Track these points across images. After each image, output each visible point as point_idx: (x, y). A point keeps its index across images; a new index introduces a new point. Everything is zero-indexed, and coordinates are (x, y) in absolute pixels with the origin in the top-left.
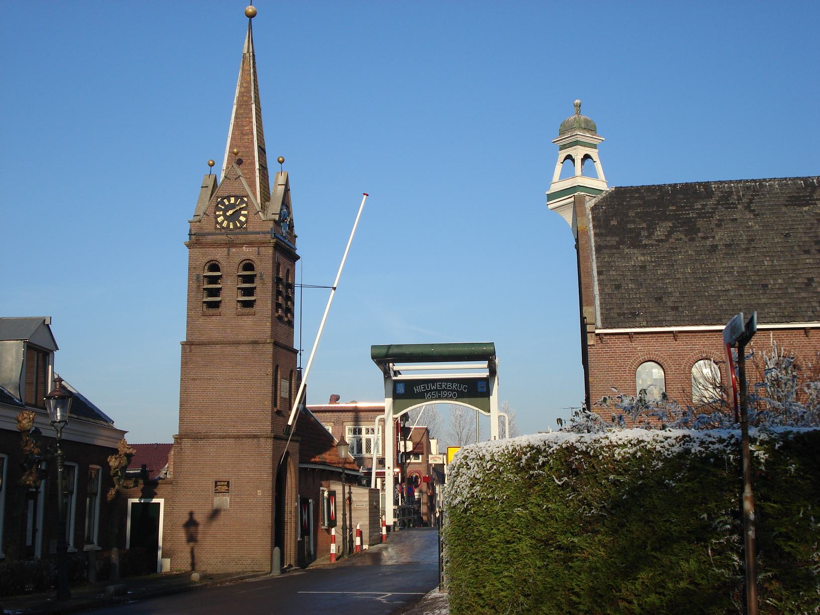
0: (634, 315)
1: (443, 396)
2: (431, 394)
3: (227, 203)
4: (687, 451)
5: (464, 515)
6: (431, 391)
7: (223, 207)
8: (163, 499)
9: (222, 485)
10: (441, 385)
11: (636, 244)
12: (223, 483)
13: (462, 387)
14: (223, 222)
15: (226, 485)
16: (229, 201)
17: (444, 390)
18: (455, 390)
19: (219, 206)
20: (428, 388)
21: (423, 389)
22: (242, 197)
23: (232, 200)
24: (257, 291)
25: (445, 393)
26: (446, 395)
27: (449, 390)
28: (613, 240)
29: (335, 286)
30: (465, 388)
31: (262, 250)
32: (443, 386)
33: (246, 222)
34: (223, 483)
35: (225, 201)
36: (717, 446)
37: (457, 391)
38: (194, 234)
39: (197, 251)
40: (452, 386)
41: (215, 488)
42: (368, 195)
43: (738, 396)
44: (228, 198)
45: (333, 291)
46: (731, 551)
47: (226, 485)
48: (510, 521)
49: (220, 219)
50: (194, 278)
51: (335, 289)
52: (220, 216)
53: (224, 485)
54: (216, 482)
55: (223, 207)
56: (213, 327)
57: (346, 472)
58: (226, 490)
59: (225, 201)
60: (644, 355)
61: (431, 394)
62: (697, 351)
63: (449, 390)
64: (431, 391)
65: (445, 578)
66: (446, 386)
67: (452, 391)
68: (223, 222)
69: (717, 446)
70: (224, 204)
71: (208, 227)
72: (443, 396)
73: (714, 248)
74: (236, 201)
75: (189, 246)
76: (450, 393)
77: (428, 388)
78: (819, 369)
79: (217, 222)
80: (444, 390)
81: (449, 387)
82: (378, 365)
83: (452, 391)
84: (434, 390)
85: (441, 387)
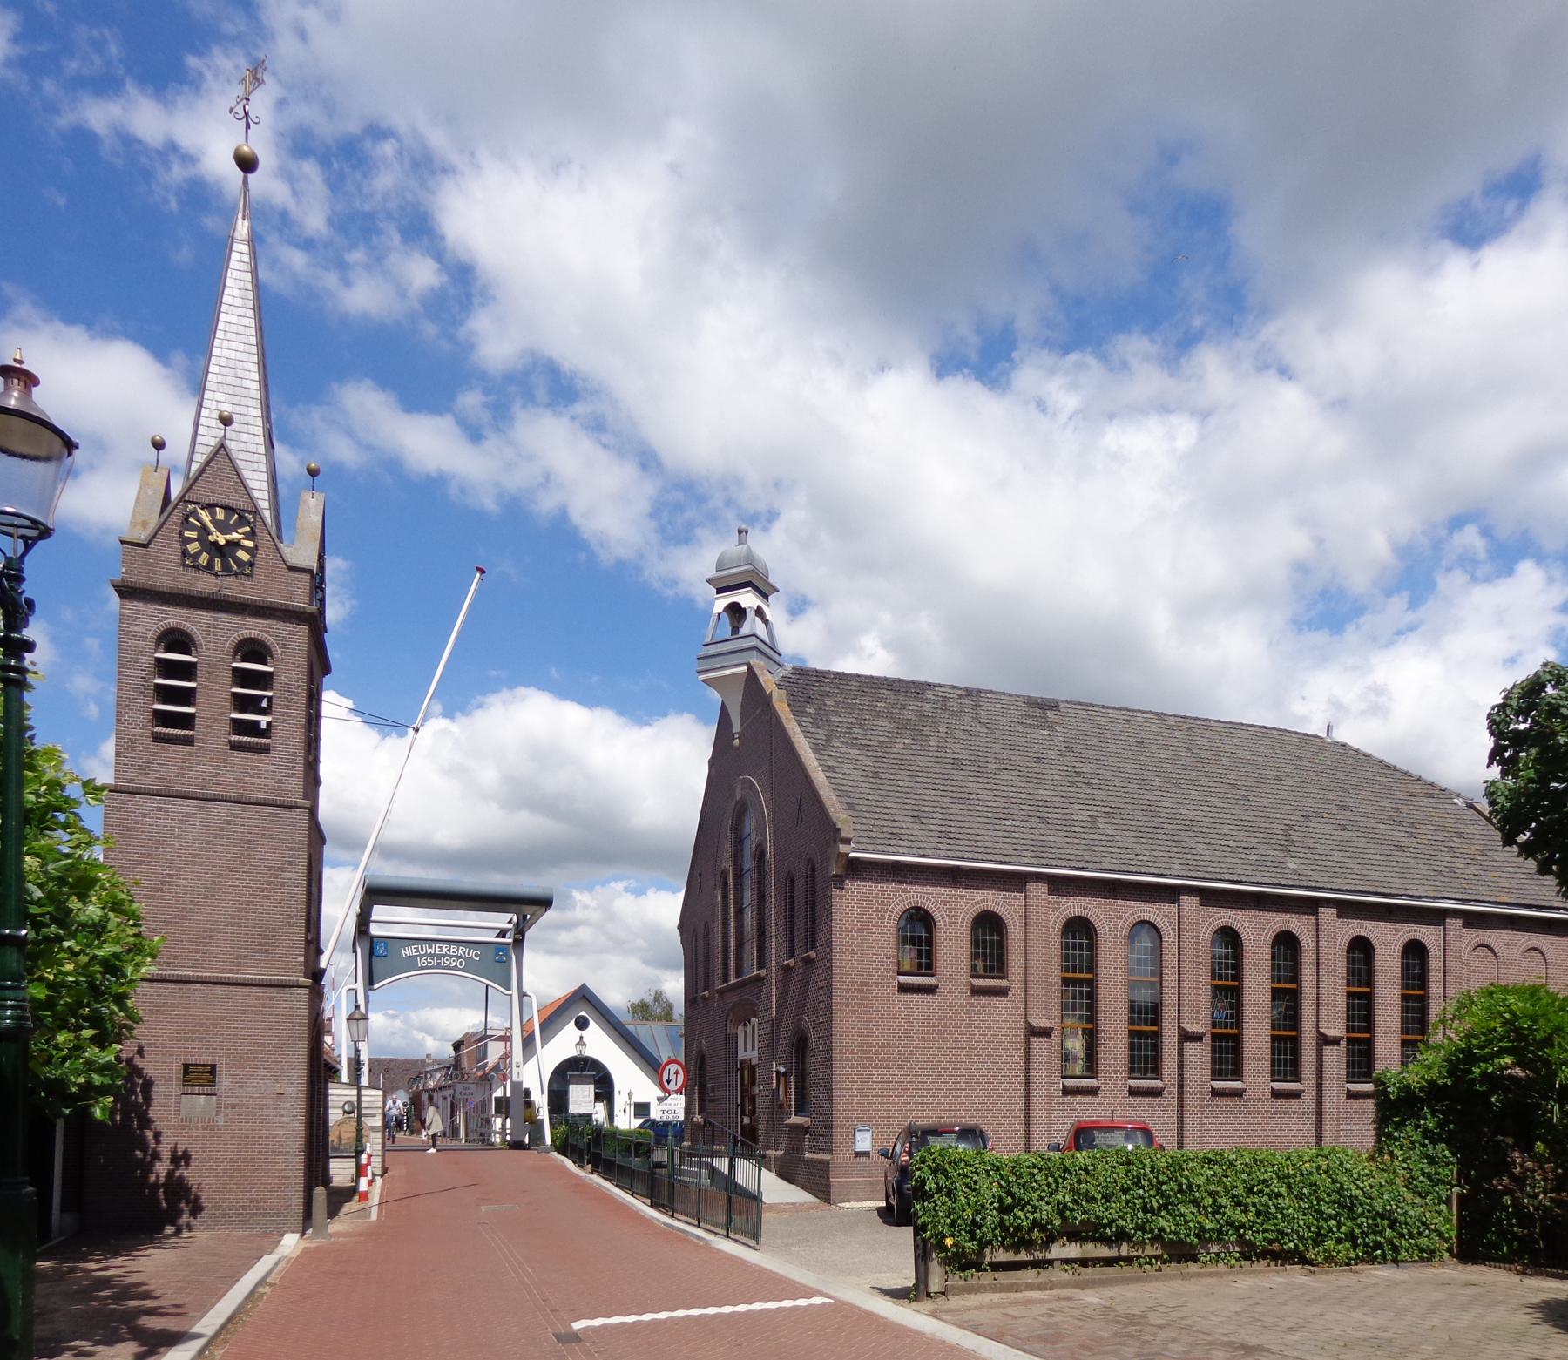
1: (433, 959)
2: (426, 960)
5: (1314, 1159)
9: (199, 1072)
10: (441, 948)
12: (201, 1069)
13: (473, 953)
14: (198, 555)
15: (207, 1072)
18: (460, 957)
19: (191, 519)
20: (469, 954)
21: (416, 952)
27: (454, 956)
30: (476, 955)
32: (445, 950)
34: (201, 1069)
36: (790, 1241)
37: (464, 958)
40: (458, 950)
41: (184, 1077)
46: (1519, 763)
47: (207, 1072)
48: (1338, 1185)
52: (192, 540)
54: (186, 1066)
56: (172, 765)
58: (210, 1081)
60: (888, 919)
61: (426, 960)
62: (979, 899)
63: (451, 957)
64: (427, 955)
66: (449, 950)
68: (198, 555)
69: (790, 1241)
77: (469, 954)
79: (185, 553)
81: (453, 952)
83: (458, 957)
84: (431, 954)
85: (442, 951)
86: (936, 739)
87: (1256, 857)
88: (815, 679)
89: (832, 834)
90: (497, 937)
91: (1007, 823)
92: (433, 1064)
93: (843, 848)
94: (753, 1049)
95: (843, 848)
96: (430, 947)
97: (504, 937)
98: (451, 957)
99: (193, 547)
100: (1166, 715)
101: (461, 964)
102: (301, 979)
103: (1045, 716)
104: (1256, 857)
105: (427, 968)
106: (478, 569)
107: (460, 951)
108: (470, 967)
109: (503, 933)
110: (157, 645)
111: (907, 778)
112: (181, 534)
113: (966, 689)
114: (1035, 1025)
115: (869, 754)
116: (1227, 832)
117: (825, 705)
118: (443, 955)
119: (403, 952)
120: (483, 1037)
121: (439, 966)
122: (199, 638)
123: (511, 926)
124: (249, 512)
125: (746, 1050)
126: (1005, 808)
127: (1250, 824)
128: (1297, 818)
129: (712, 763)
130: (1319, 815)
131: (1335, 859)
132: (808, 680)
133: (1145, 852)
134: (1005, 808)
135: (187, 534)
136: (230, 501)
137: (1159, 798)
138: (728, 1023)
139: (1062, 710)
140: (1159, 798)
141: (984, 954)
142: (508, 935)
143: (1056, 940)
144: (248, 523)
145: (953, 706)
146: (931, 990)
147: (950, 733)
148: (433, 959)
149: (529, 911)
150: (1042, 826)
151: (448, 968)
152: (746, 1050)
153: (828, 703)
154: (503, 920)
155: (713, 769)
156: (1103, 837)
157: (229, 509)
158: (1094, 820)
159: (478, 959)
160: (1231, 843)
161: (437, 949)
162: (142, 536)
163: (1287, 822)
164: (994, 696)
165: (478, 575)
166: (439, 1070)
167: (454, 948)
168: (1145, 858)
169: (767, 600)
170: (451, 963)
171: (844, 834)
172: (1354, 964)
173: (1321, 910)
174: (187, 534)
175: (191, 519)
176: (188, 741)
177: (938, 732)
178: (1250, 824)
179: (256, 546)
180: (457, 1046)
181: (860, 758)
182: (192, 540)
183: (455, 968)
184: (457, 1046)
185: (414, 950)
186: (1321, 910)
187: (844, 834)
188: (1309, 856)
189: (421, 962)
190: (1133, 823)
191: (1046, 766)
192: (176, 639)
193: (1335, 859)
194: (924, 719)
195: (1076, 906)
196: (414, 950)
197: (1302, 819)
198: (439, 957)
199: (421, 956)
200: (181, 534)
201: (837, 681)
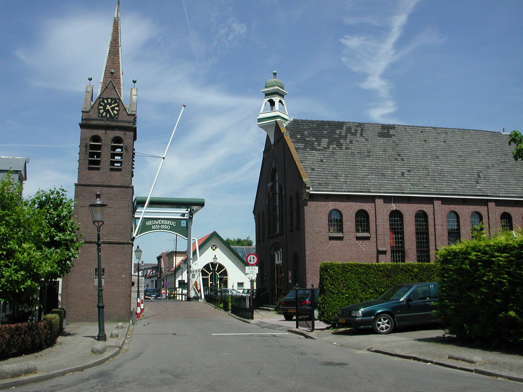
0: (327, 184)
1: (158, 226)
3: (106, 102)
6: (155, 224)
7: (103, 104)
10: (161, 222)
11: (313, 149)
13: (173, 223)
14: (103, 113)
16: (107, 101)
17: (163, 224)
18: (168, 225)
19: (101, 103)
22: (115, 100)
23: (109, 101)
28: (302, 146)
29: (164, 157)
31: (128, 133)
32: (162, 222)
33: (118, 114)
35: (105, 101)
37: (170, 225)
38: (85, 120)
39: (86, 131)
42: (185, 106)
44: (107, 99)
49: (102, 111)
50: (83, 145)
52: (101, 109)
55: (103, 104)
56: (95, 177)
59: (105, 101)
63: (165, 225)
64: (155, 224)
65: (488, 358)
66: (164, 222)
67: (167, 225)
68: (103, 113)
70: (104, 102)
71: (94, 115)
73: (353, 154)
74: (112, 101)
75: (82, 126)
78: (1, 226)
79: (99, 113)
80: (163, 224)
82: (181, 208)
83: (167, 225)
84: (157, 224)
85: (161, 222)
86: (345, 145)
87: (465, 184)
88: (301, 123)
89: (304, 186)
90: (180, 216)
91: (369, 177)
92: (144, 266)
93: (307, 191)
94: (281, 260)
95: (307, 191)
96: (157, 221)
97: (184, 216)
98: (165, 225)
99: (102, 111)
100: (437, 128)
101: (168, 227)
102: (130, 241)
103: (388, 132)
104: (465, 184)
105: (156, 229)
106: (183, 105)
107: (168, 223)
108: (172, 229)
109: (183, 215)
110: (90, 141)
111: (333, 161)
112: (98, 108)
113: (359, 123)
114: (380, 250)
115: (319, 152)
116: (455, 175)
117: (304, 134)
118: (161, 224)
119: (147, 223)
120: (172, 255)
121: (160, 229)
122: (103, 138)
123: (187, 212)
124: (118, 99)
125: (278, 261)
126: (369, 171)
127: (464, 171)
128: (484, 168)
129: (265, 152)
130: (493, 166)
131: (496, 183)
132: (298, 124)
133: (421, 185)
134: (369, 171)
135: (100, 107)
136: (113, 97)
137: (430, 163)
138: (272, 250)
139: (396, 128)
140: (430, 163)
141: (361, 225)
142: (186, 215)
143: (387, 217)
144: (117, 102)
145: (353, 131)
146: (340, 239)
147: (351, 142)
148: (158, 226)
149: (195, 208)
150: (383, 177)
151: (164, 229)
152: (278, 261)
153: (305, 133)
154: (184, 211)
155: (265, 155)
156: (406, 180)
157: (112, 99)
158: (403, 174)
159: (175, 225)
160: (456, 180)
161: (160, 222)
162: (87, 110)
163: (480, 170)
164: (370, 125)
165: (183, 108)
166: (149, 269)
167: (166, 221)
168: (421, 187)
169: (283, 97)
170: (165, 227)
171: (307, 186)
172: (418, 239)
173: (489, 204)
174: (100, 107)
175: (101, 103)
176: (98, 169)
177: (347, 142)
178: (464, 171)
179: (119, 109)
180: (159, 258)
181: (316, 154)
182: (101, 109)
183: (166, 229)
184: (159, 258)
185: (151, 223)
186: (489, 204)
187: (307, 186)
188: (486, 183)
189: (153, 227)
190: (418, 174)
191: (387, 153)
192: (96, 138)
193: (496, 183)
194: (341, 137)
195: (394, 207)
196: (151, 223)
197: (486, 168)
198: (160, 225)
199: (153, 225)
200: (98, 108)
201: (309, 123)
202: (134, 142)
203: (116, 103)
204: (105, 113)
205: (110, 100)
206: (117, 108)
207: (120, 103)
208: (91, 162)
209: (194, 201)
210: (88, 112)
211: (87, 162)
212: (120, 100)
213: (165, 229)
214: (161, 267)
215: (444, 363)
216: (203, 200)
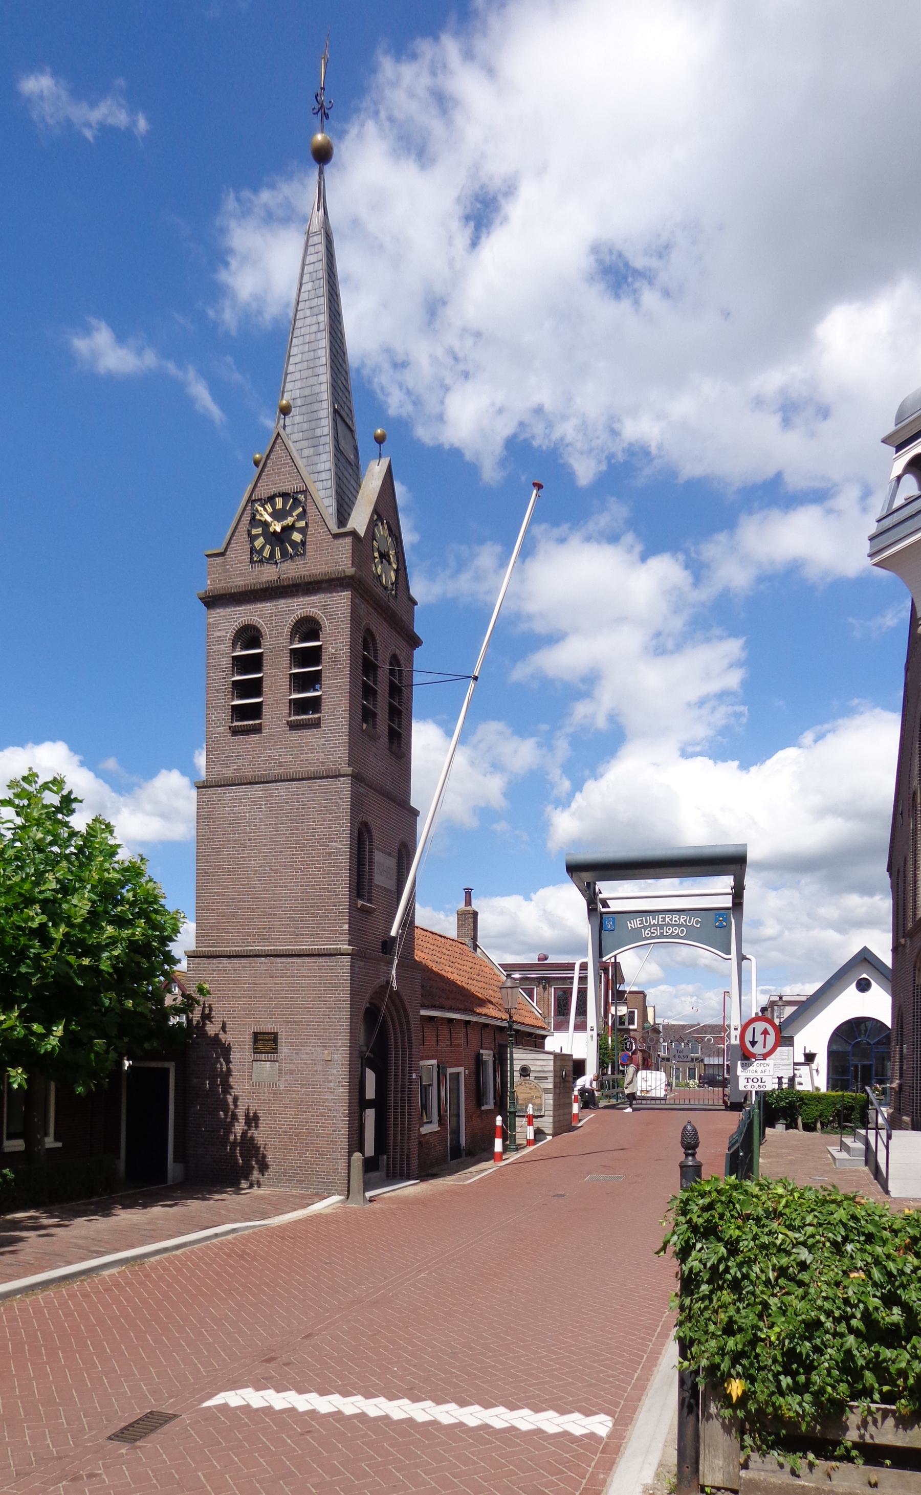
1: (656, 930)
4: (247, 1179)
8: (173, 1064)
10: (664, 918)
12: (266, 1037)
13: (693, 921)
14: (263, 547)
17: (667, 925)
18: (682, 925)
20: (647, 923)
24: (326, 681)
25: (669, 929)
26: (670, 931)
30: (697, 922)
32: (667, 919)
40: (679, 919)
43: (251, 1231)
45: (472, 685)
51: (476, 678)
53: (270, 1040)
57: (516, 1027)
64: (651, 926)
66: (671, 920)
67: (679, 926)
68: (263, 547)
72: (667, 932)
74: (285, 504)
76: (676, 929)
77: (647, 923)
80: (667, 925)
81: (675, 921)
101: (682, 931)
105: (651, 938)
112: (249, 532)
119: (629, 925)
121: (662, 936)
135: (254, 532)
148: (656, 930)
161: (660, 920)
167: (675, 917)
170: (673, 932)
174: (254, 532)
183: (677, 936)
185: (638, 922)
198: (662, 927)
199: (645, 928)
202: (700, 758)
203: (298, 508)
204: (268, 546)
205: (281, 499)
206: (302, 524)
207: (311, 509)
208: (240, 712)
209: (718, 851)
210: (222, 554)
211: (227, 715)
212: (309, 497)
213: (674, 937)
214: (350, 952)
215: (327, 959)
216: (740, 849)
